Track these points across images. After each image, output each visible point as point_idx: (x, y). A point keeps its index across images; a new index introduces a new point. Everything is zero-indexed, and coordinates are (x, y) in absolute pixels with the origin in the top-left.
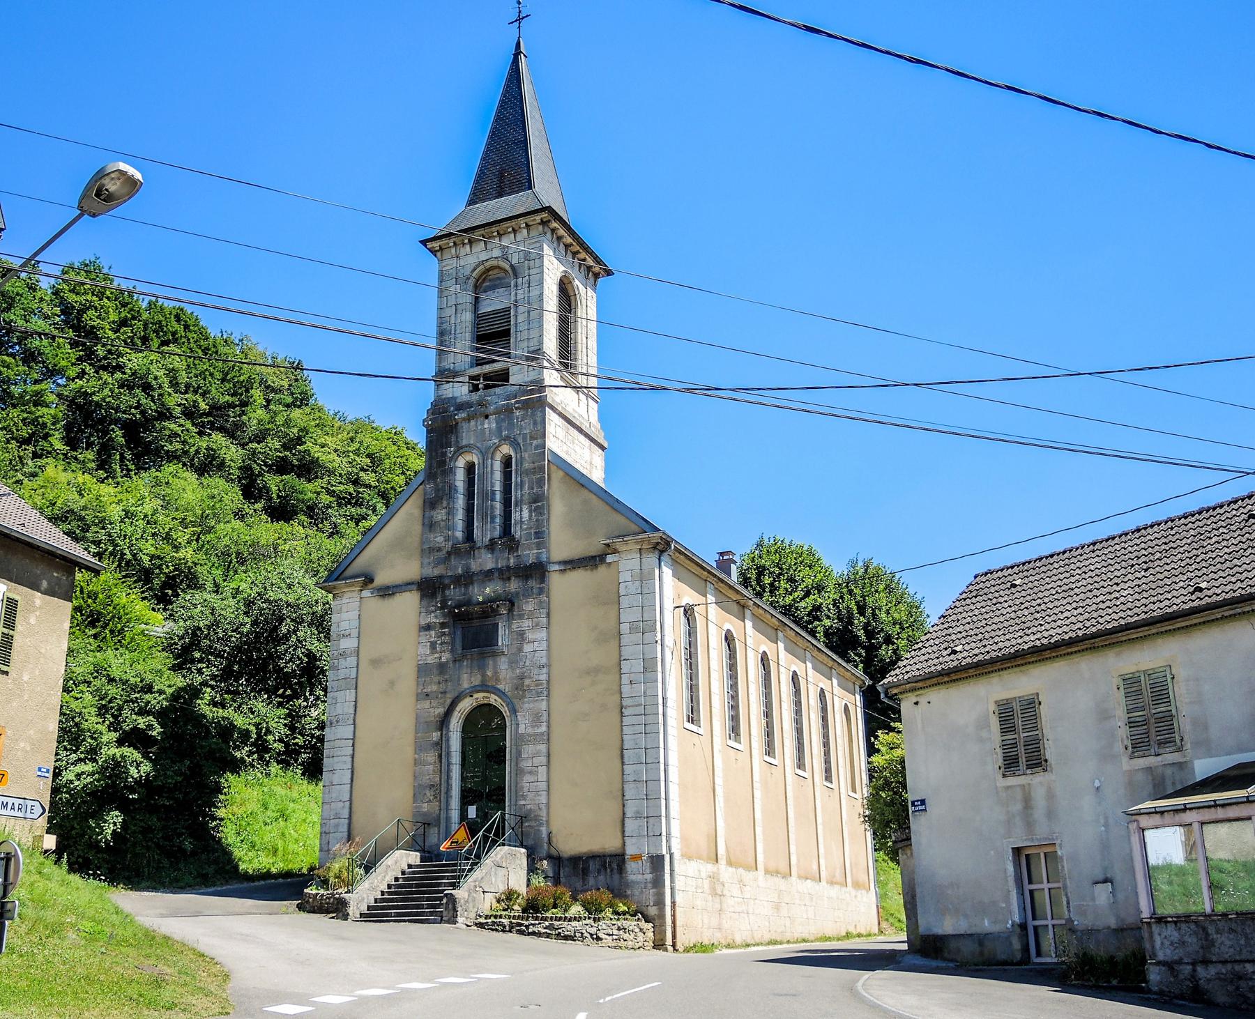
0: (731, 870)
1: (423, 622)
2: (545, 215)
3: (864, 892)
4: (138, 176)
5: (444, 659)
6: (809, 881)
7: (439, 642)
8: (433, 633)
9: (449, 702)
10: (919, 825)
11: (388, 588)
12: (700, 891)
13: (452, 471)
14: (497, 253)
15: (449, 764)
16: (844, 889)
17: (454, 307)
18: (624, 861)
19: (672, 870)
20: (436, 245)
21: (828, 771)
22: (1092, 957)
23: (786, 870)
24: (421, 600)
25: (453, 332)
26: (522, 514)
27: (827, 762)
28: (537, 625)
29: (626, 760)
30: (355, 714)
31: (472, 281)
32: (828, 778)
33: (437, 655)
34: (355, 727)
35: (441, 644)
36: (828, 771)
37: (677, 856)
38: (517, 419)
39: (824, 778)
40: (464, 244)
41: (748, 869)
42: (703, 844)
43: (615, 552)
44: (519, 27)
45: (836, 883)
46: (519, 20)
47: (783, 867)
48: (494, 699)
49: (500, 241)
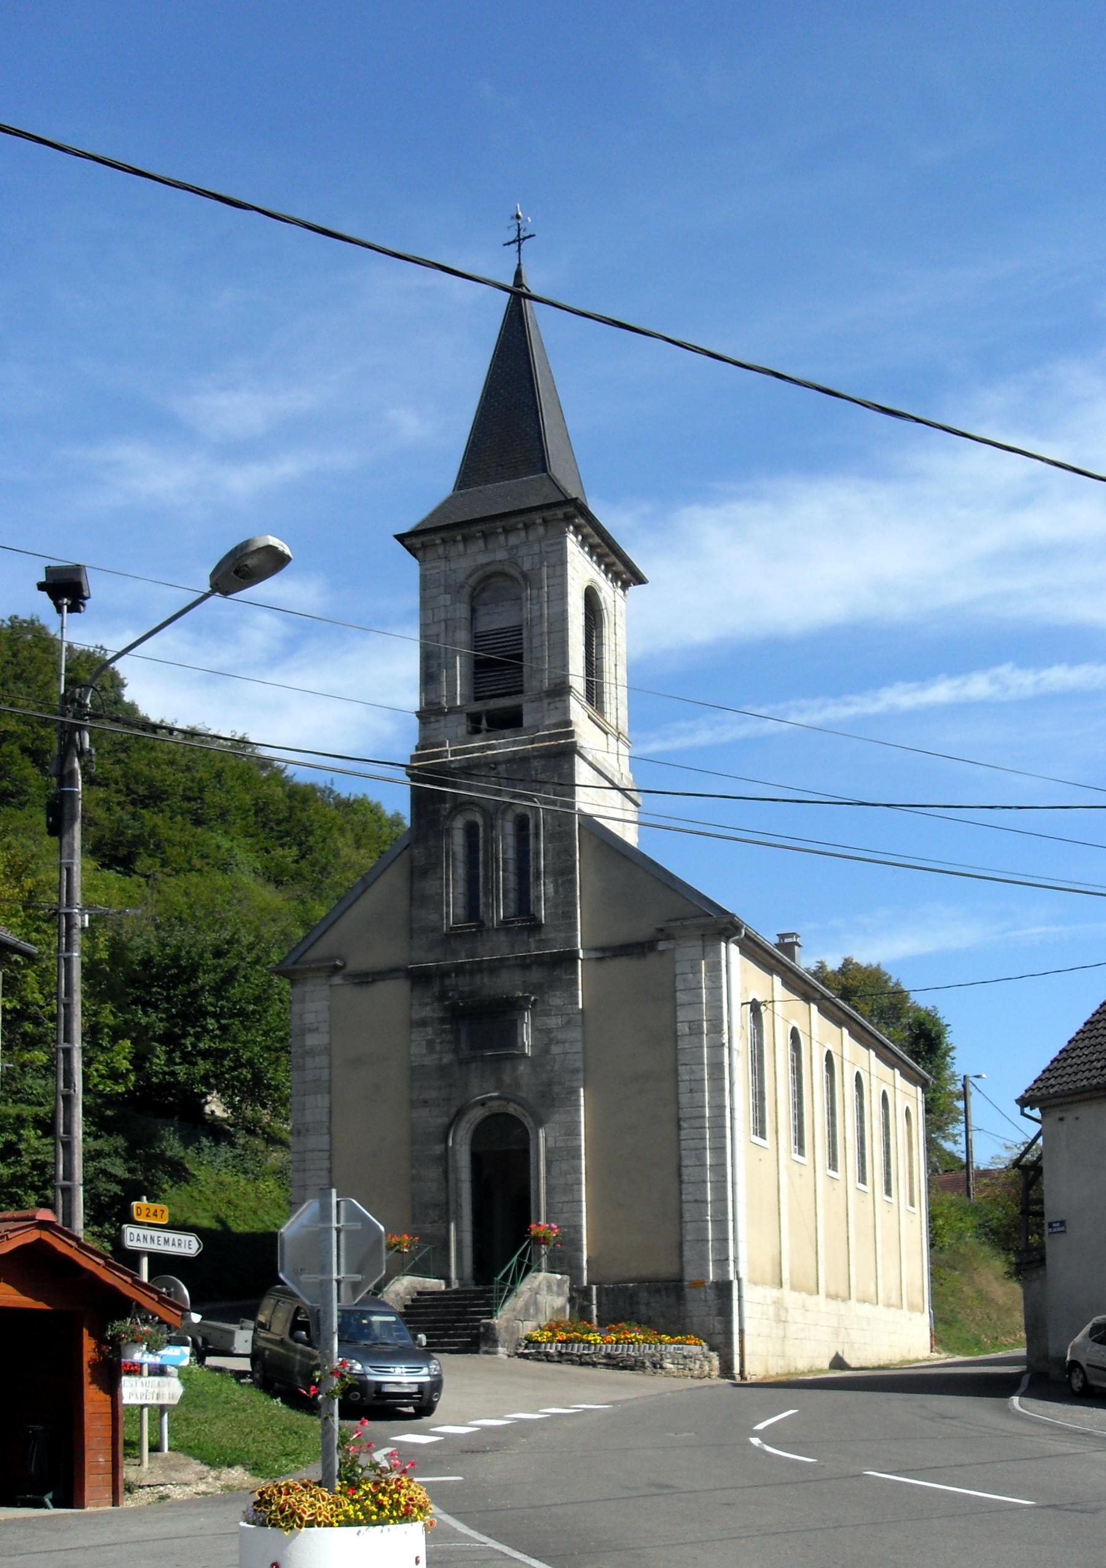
0: (795, 1294)
1: (416, 1016)
2: (570, 510)
3: (919, 1314)
4: (287, 551)
5: (445, 1061)
6: (867, 1304)
7: (438, 1041)
8: (430, 1030)
9: (454, 1110)
10: (1057, 1250)
11: (366, 975)
12: (765, 1317)
13: (448, 833)
14: (501, 555)
15: (458, 1181)
16: (899, 1311)
17: (443, 624)
18: (682, 1289)
19: (740, 1297)
20: (417, 542)
21: (888, 1183)
22: (264, 1392)
23: (844, 1293)
24: (412, 990)
25: (443, 656)
26: (544, 889)
27: (888, 1174)
28: (568, 1023)
29: (685, 1178)
30: (330, 1122)
31: (467, 591)
32: (888, 1192)
33: (435, 1056)
34: (331, 1137)
35: (441, 1043)
36: (888, 1183)
37: (745, 1283)
38: (536, 770)
39: (884, 1192)
40: (455, 541)
41: (810, 1293)
42: (768, 1269)
43: (669, 937)
44: (519, 250)
45: (893, 1306)
46: (519, 240)
47: (843, 1291)
48: (512, 1109)
49: (506, 539)
